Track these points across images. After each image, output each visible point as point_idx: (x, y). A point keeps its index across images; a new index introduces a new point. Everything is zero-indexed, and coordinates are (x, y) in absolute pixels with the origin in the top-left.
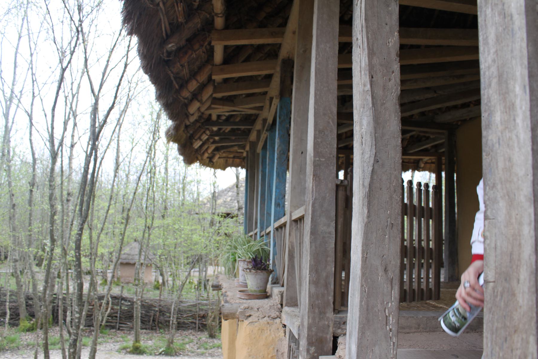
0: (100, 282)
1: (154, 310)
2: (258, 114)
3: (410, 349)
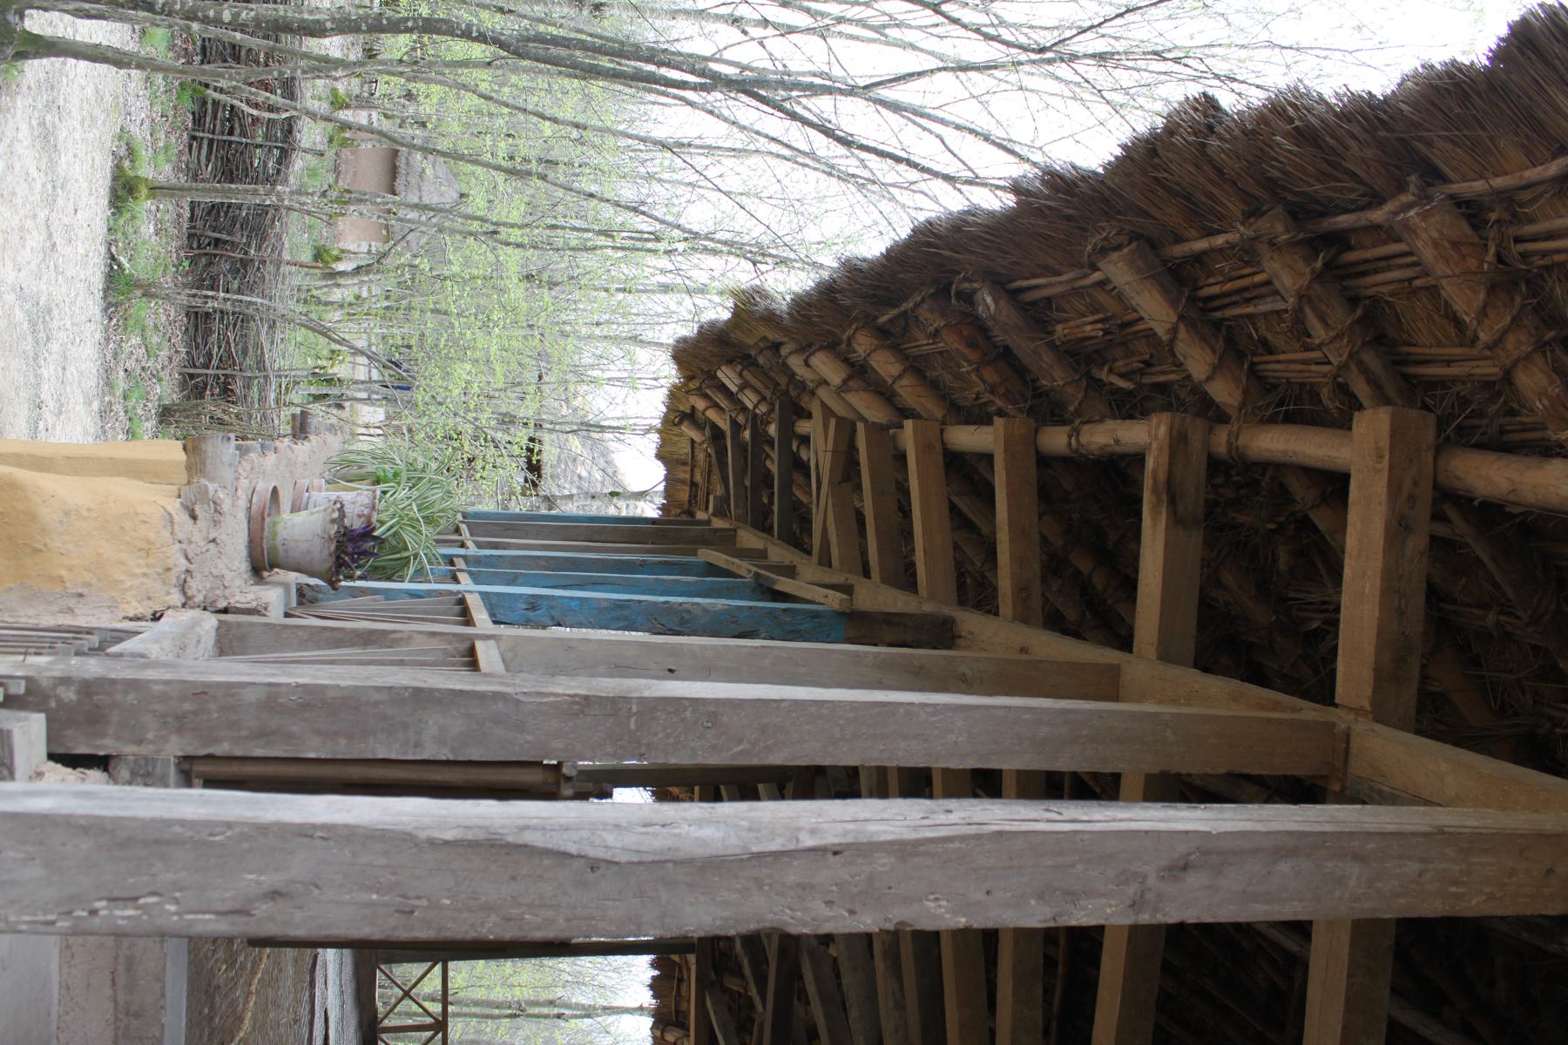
0: (341, 87)
1: (249, 245)
2: (809, 553)
3: (56, 988)
